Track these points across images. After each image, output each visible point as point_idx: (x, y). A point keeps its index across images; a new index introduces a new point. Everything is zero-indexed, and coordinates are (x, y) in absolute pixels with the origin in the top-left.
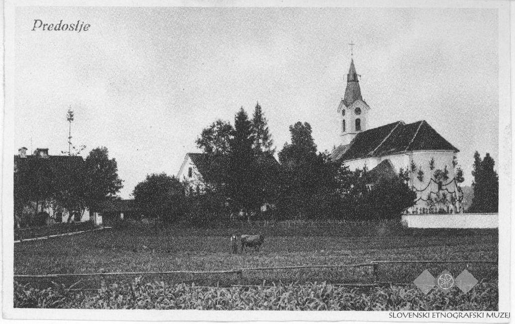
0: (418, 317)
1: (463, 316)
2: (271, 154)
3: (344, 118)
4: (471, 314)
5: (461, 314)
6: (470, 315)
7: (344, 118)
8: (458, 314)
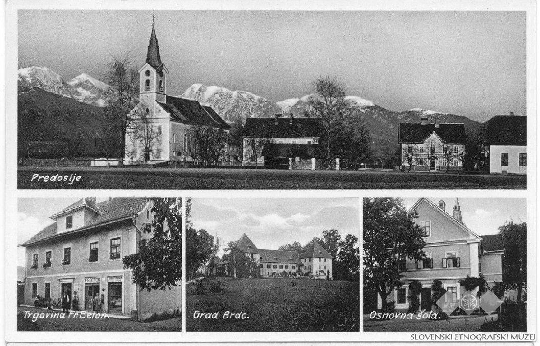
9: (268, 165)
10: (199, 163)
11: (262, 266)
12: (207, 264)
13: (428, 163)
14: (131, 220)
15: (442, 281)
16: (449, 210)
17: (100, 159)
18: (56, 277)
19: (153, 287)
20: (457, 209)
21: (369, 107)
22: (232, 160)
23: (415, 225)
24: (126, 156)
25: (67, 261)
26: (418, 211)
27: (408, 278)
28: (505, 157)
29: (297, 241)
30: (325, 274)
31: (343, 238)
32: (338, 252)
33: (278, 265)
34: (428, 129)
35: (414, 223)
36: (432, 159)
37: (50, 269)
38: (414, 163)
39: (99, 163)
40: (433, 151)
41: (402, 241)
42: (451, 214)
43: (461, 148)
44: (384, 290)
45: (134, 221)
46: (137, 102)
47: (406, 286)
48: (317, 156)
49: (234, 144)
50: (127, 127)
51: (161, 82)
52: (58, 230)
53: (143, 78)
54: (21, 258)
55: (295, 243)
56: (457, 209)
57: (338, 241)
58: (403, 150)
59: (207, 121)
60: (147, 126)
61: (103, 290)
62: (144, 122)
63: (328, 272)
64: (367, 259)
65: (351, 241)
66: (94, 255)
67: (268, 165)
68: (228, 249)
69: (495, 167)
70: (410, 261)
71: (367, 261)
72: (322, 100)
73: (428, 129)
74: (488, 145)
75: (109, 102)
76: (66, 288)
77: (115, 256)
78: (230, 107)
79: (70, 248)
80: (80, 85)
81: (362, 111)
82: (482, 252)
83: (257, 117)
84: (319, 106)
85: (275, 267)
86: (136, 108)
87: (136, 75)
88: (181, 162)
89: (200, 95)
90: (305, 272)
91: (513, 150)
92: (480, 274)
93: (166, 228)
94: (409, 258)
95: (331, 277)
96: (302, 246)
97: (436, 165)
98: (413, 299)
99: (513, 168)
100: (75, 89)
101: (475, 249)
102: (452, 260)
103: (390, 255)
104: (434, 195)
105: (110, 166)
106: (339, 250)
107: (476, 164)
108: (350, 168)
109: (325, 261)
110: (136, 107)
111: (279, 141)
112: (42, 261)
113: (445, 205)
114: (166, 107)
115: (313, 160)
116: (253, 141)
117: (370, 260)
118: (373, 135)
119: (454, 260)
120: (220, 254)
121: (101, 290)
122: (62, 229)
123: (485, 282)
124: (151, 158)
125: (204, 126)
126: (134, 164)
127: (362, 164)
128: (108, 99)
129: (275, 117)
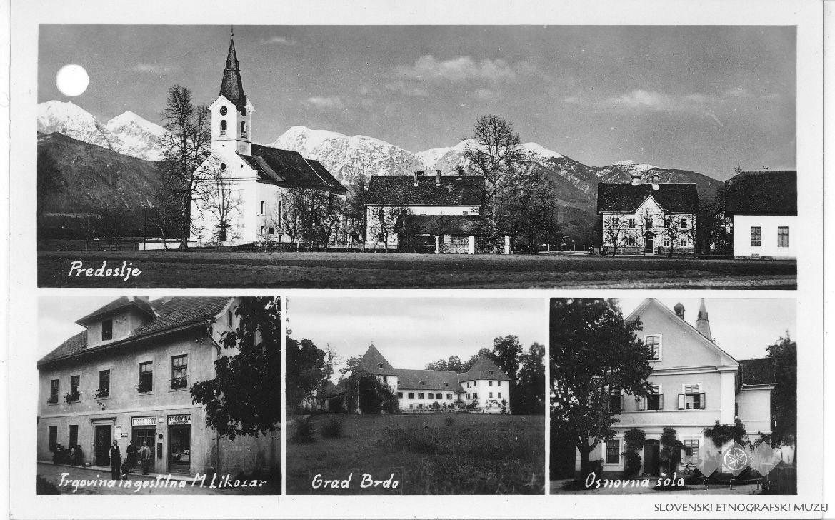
0: (695, 510)
1: (760, 508)
2: (353, 205)
3: (224, 118)
4: (772, 506)
5: (757, 506)
6: (771, 507)
7: (224, 118)
8: (753, 506)
9: (403, 248)
10: (300, 244)
11: (400, 395)
12: (315, 393)
13: (641, 242)
14: (204, 328)
15: (676, 429)
16: (691, 317)
17: (153, 239)
18: (83, 415)
19: (239, 432)
20: (703, 317)
21: (553, 159)
22: (350, 240)
23: (636, 341)
24: (191, 234)
25: (104, 391)
26: (641, 320)
27: (627, 420)
28: (757, 232)
29: (454, 356)
30: (499, 405)
31: (526, 350)
32: (518, 371)
33: (426, 393)
34: (643, 192)
35: (635, 338)
36: (649, 236)
37: (76, 405)
38: (620, 242)
39: (151, 246)
40: (649, 225)
41: (617, 366)
42: (694, 324)
43: (691, 221)
44: (586, 442)
45: (208, 329)
46: (207, 154)
47: (620, 436)
48: (477, 233)
49: (352, 216)
50: (193, 192)
51: (243, 123)
52: (89, 343)
53: (216, 119)
54: (31, 389)
55: (452, 358)
56: (703, 317)
57: (519, 354)
58: (604, 224)
59: (317, 185)
60: (223, 190)
61: (161, 436)
62: (218, 184)
63: (504, 402)
64: (560, 393)
65: (538, 352)
66: (146, 383)
67: (403, 248)
68: (348, 370)
69: (742, 248)
70: (629, 399)
71: (560, 396)
72: (485, 149)
73: (643, 192)
74: (730, 215)
75: (166, 153)
76: (101, 433)
77: (177, 384)
78: (348, 161)
79: (108, 371)
80: (122, 129)
81: (546, 165)
82: (741, 385)
83: (387, 174)
84: (480, 158)
85: (421, 396)
86: (205, 163)
87: (205, 112)
88: (273, 243)
89: (301, 143)
90: (468, 402)
91: (770, 224)
92: (736, 421)
93: (258, 340)
94: (626, 392)
95: (508, 409)
96: (463, 362)
97: (655, 245)
98: (631, 457)
99: (770, 249)
100: (114, 135)
101: (729, 381)
102: (692, 398)
103: (597, 387)
104: (668, 298)
105: (168, 250)
106: (521, 366)
107: (714, 244)
108: (526, 252)
109: (499, 385)
110: (206, 161)
111: (417, 211)
112: (65, 389)
113: (684, 311)
114: (250, 161)
115: (472, 239)
116: (382, 212)
117: (565, 395)
118: (560, 202)
119: (696, 397)
120: (335, 379)
121: (157, 437)
122: (96, 341)
123: (744, 432)
124: (229, 236)
125: (308, 190)
126: (203, 246)
127: (544, 245)
128: (164, 150)
129: (413, 175)
